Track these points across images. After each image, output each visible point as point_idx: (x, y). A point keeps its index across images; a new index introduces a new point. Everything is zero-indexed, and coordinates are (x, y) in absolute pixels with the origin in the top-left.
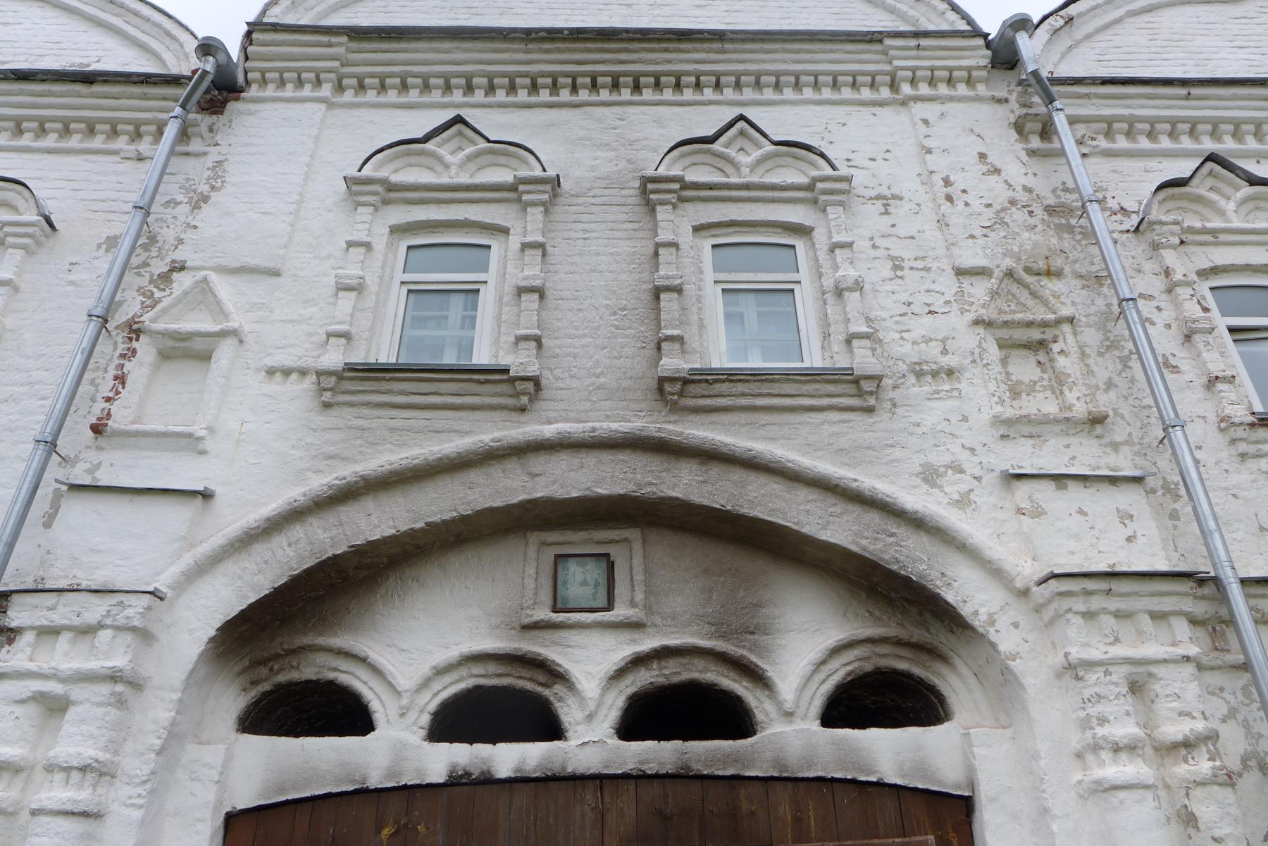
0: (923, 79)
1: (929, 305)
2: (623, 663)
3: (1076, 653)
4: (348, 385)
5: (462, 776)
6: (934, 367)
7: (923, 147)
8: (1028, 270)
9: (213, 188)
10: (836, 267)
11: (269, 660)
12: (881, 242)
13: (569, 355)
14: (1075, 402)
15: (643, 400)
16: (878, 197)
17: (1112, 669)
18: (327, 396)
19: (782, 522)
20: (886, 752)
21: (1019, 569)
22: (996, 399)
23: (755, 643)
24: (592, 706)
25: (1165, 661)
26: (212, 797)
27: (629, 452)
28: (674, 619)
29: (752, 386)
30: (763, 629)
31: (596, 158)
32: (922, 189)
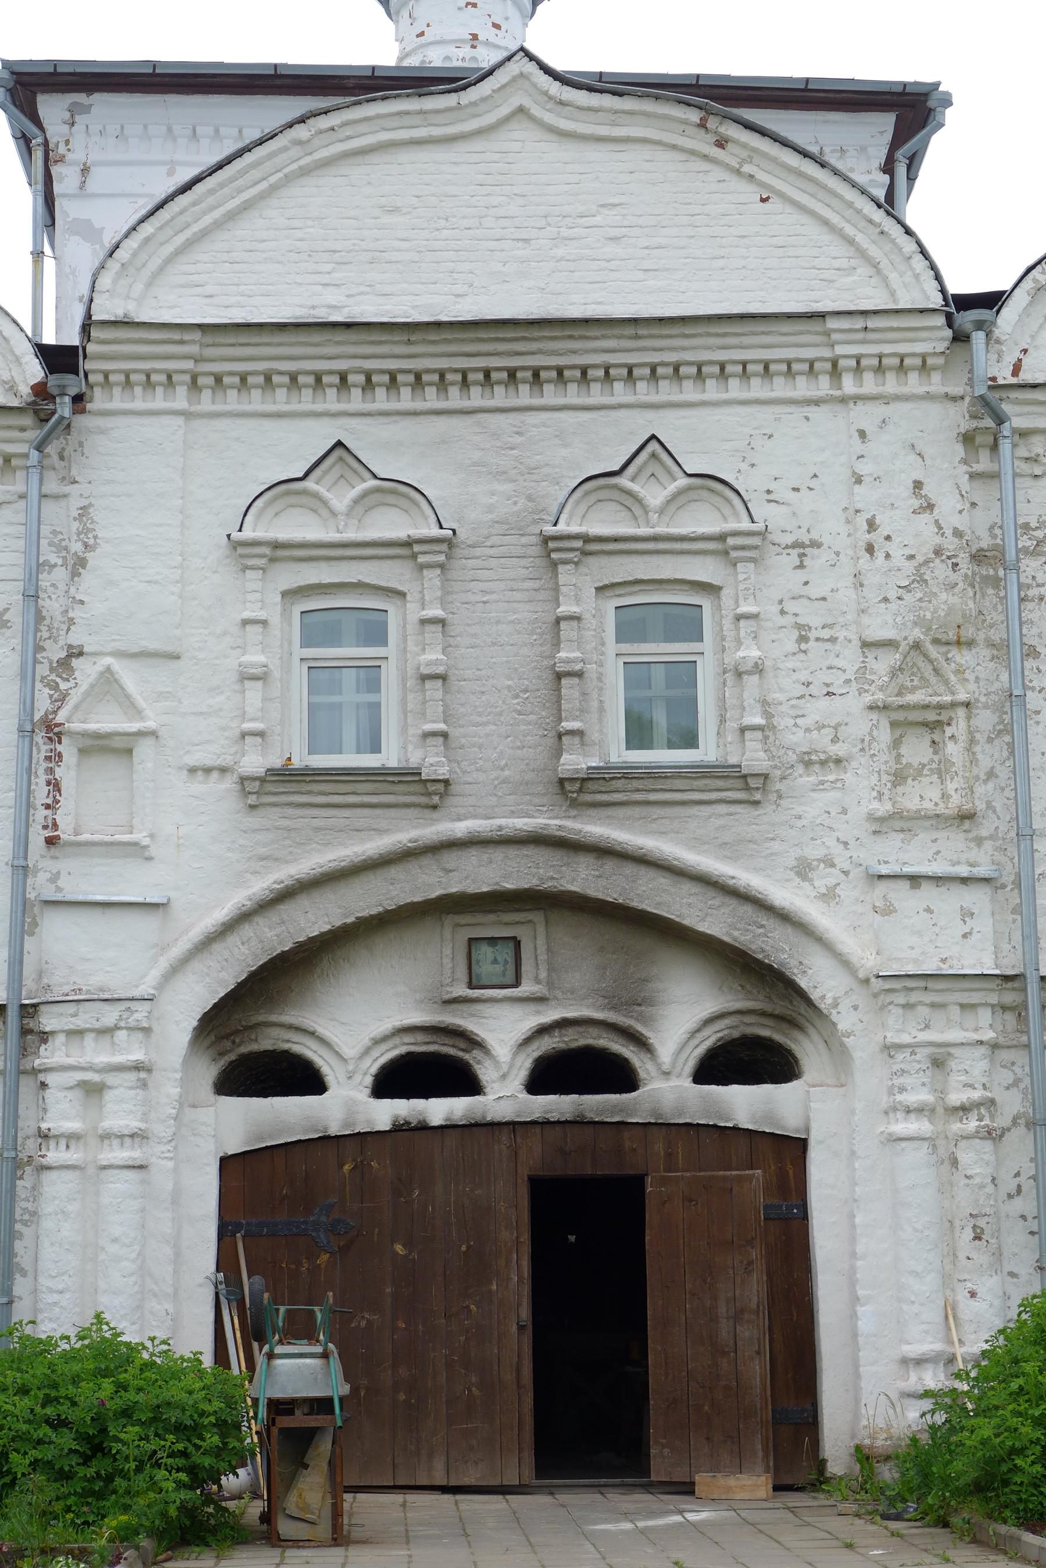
0: (870, 368)
1: (827, 685)
2: (530, 1033)
3: (892, 1038)
4: (269, 787)
5: (403, 1125)
6: (823, 757)
7: (854, 473)
8: (936, 641)
9: (86, 546)
10: (739, 643)
11: (231, 1035)
12: (790, 607)
13: (474, 745)
14: (953, 793)
15: (544, 794)
16: (796, 545)
17: (917, 1050)
18: (252, 800)
19: (665, 914)
20: (743, 1104)
21: (863, 962)
22: (875, 794)
23: (641, 1013)
24: (505, 1068)
25: (962, 1044)
26: (212, 1147)
27: (532, 846)
28: (572, 993)
29: (645, 782)
30: (648, 1001)
31: (493, 494)
32: (844, 529)
